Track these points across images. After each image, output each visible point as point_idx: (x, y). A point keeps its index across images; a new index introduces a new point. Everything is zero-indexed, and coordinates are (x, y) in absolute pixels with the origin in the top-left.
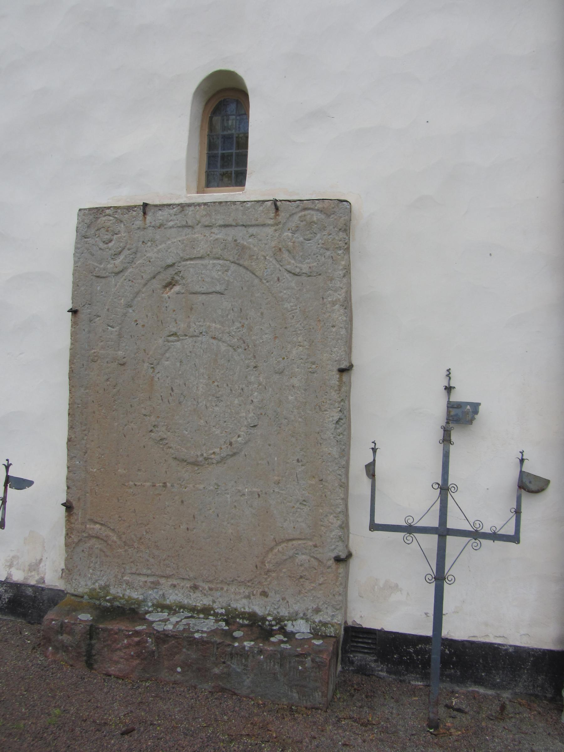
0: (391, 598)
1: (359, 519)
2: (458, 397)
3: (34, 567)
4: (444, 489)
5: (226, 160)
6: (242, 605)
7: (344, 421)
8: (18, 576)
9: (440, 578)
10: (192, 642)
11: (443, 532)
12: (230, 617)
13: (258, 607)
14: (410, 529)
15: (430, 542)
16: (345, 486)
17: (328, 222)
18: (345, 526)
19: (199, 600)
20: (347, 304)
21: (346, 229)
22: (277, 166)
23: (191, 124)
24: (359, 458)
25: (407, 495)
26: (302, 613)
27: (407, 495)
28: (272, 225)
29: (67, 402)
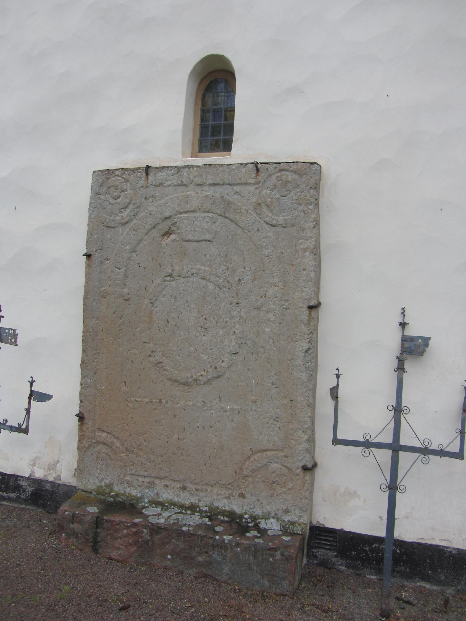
0: (350, 502)
1: (324, 435)
2: (411, 332)
3: (53, 466)
4: (398, 411)
5: (216, 131)
6: (223, 504)
7: (312, 351)
8: (39, 474)
9: (393, 488)
10: (180, 534)
11: (396, 448)
12: (213, 514)
13: (237, 507)
14: (367, 444)
15: (385, 456)
16: (312, 406)
17: (300, 183)
18: (311, 440)
19: (187, 499)
20: (316, 251)
21: (316, 187)
22: (260, 135)
23: (186, 111)
24: (325, 383)
25: (366, 415)
26: (273, 512)
27: (366, 415)
28: (253, 184)
29: (81, 330)
